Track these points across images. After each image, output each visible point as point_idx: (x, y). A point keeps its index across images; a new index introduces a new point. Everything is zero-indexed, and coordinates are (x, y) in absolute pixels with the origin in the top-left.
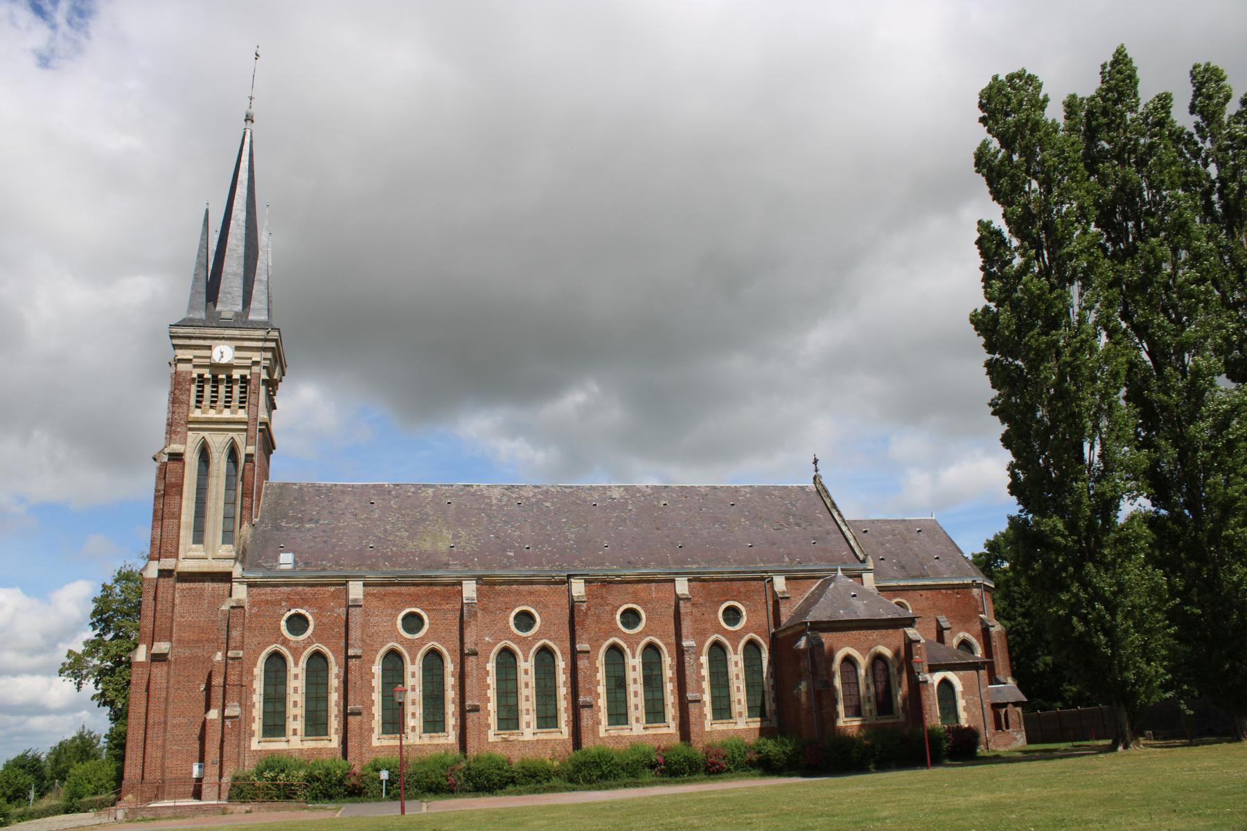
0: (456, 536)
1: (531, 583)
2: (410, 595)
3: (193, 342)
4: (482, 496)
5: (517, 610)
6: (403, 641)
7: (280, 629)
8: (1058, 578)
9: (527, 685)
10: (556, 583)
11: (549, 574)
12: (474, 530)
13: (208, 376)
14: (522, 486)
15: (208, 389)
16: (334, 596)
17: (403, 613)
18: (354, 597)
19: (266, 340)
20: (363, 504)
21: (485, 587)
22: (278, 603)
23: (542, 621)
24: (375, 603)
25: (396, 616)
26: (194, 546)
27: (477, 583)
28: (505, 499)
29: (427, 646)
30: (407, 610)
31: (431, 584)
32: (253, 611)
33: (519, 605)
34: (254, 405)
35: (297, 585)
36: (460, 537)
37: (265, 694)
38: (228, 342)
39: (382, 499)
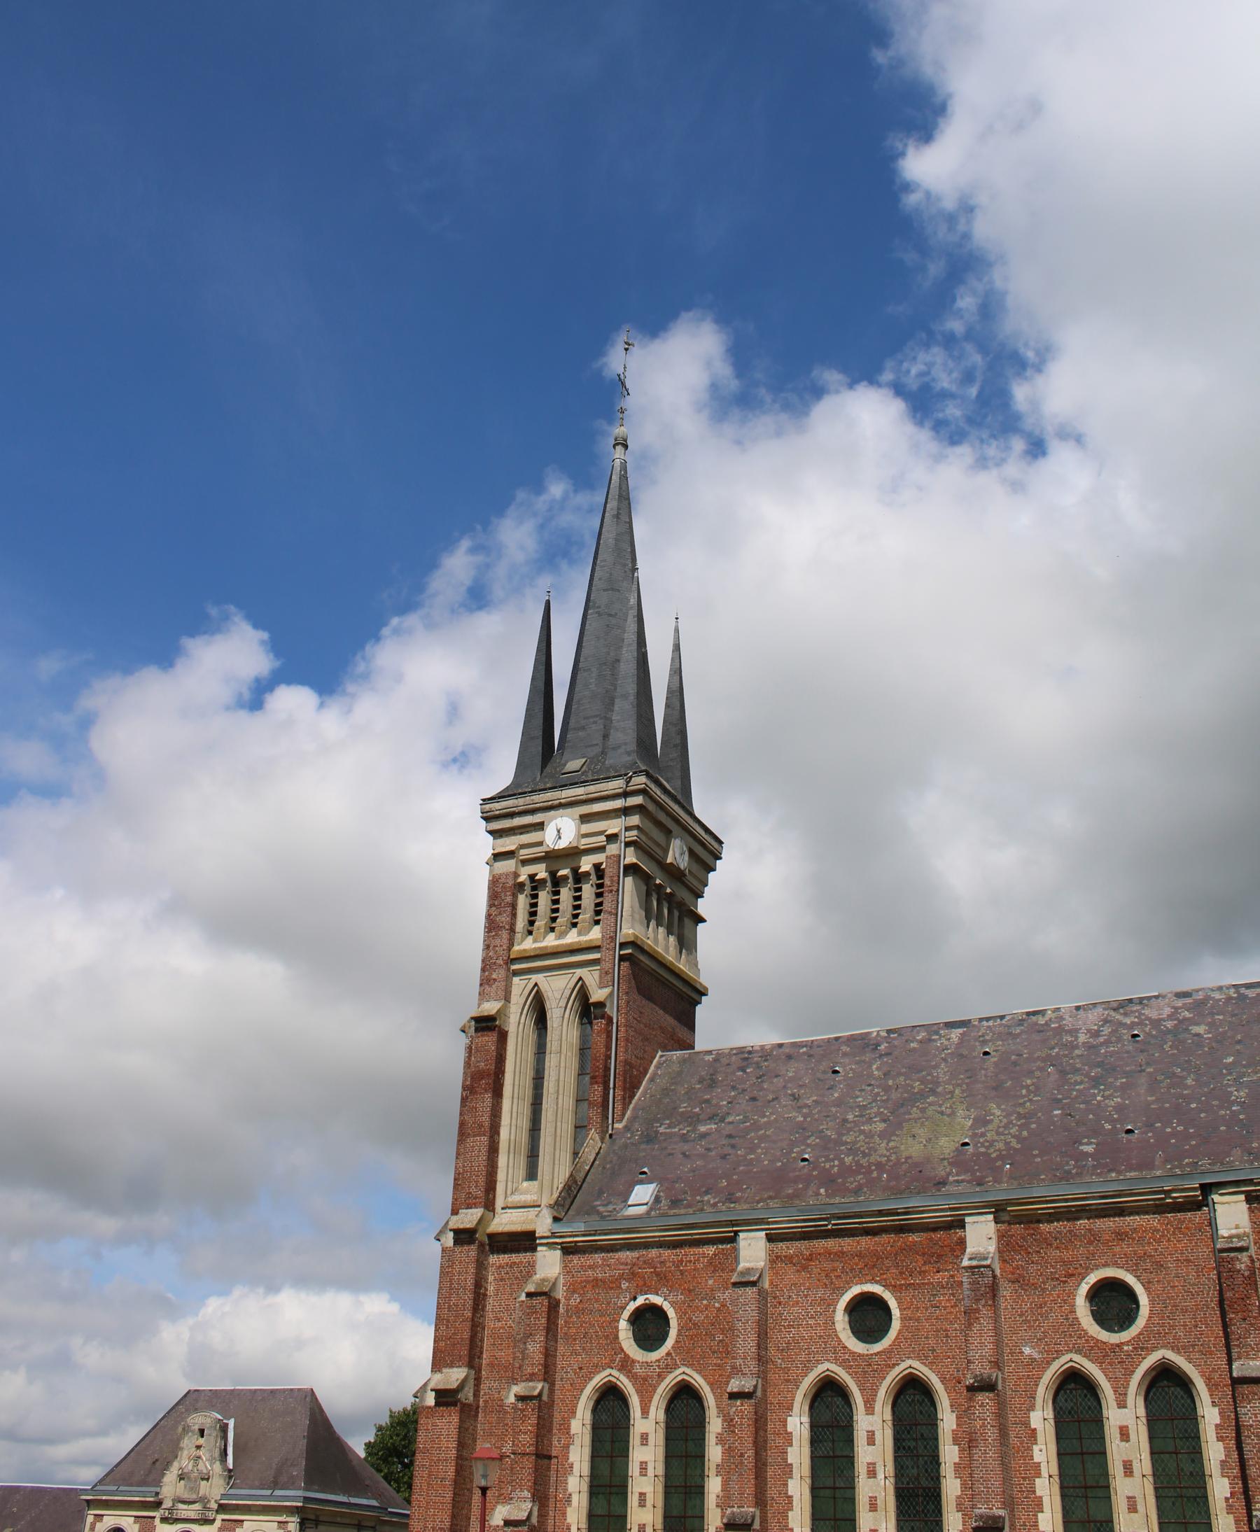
0: (981, 1121)
1: (1121, 1211)
2: (860, 1255)
3: (518, 821)
4: (1060, 1030)
5: (1092, 1278)
6: (850, 1360)
7: (617, 1337)
8: (1256, 1015)
9: (1128, 1469)
10: (1178, 1207)
11: (1156, 1185)
12: (1022, 1105)
13: (542, 875)
14: (1149, 998)
15: (544, 898)
16: (715, 1266)
17: (848, 1297)
18: (748, 1265)
19: (626, 794)
20: (819, 1075)
21: (1018, 1229)
22: (612, 1285)
23: (1152, 1302)
24: (791, 1275)
25: (833, 1303)
26: (525, 1184)
27: (997, 1221)
28: (1106, 1030)
29: (897, 1370)
30: (856, 1290)
31: (901, 1229)
32: (572, 1302)
33: (1097, 1267)
34: (610, 913)
35: (647, 1245)
36: (991, 1121)
37: (593, 1476)
38: (569, 811)
39: (857, 1063)
